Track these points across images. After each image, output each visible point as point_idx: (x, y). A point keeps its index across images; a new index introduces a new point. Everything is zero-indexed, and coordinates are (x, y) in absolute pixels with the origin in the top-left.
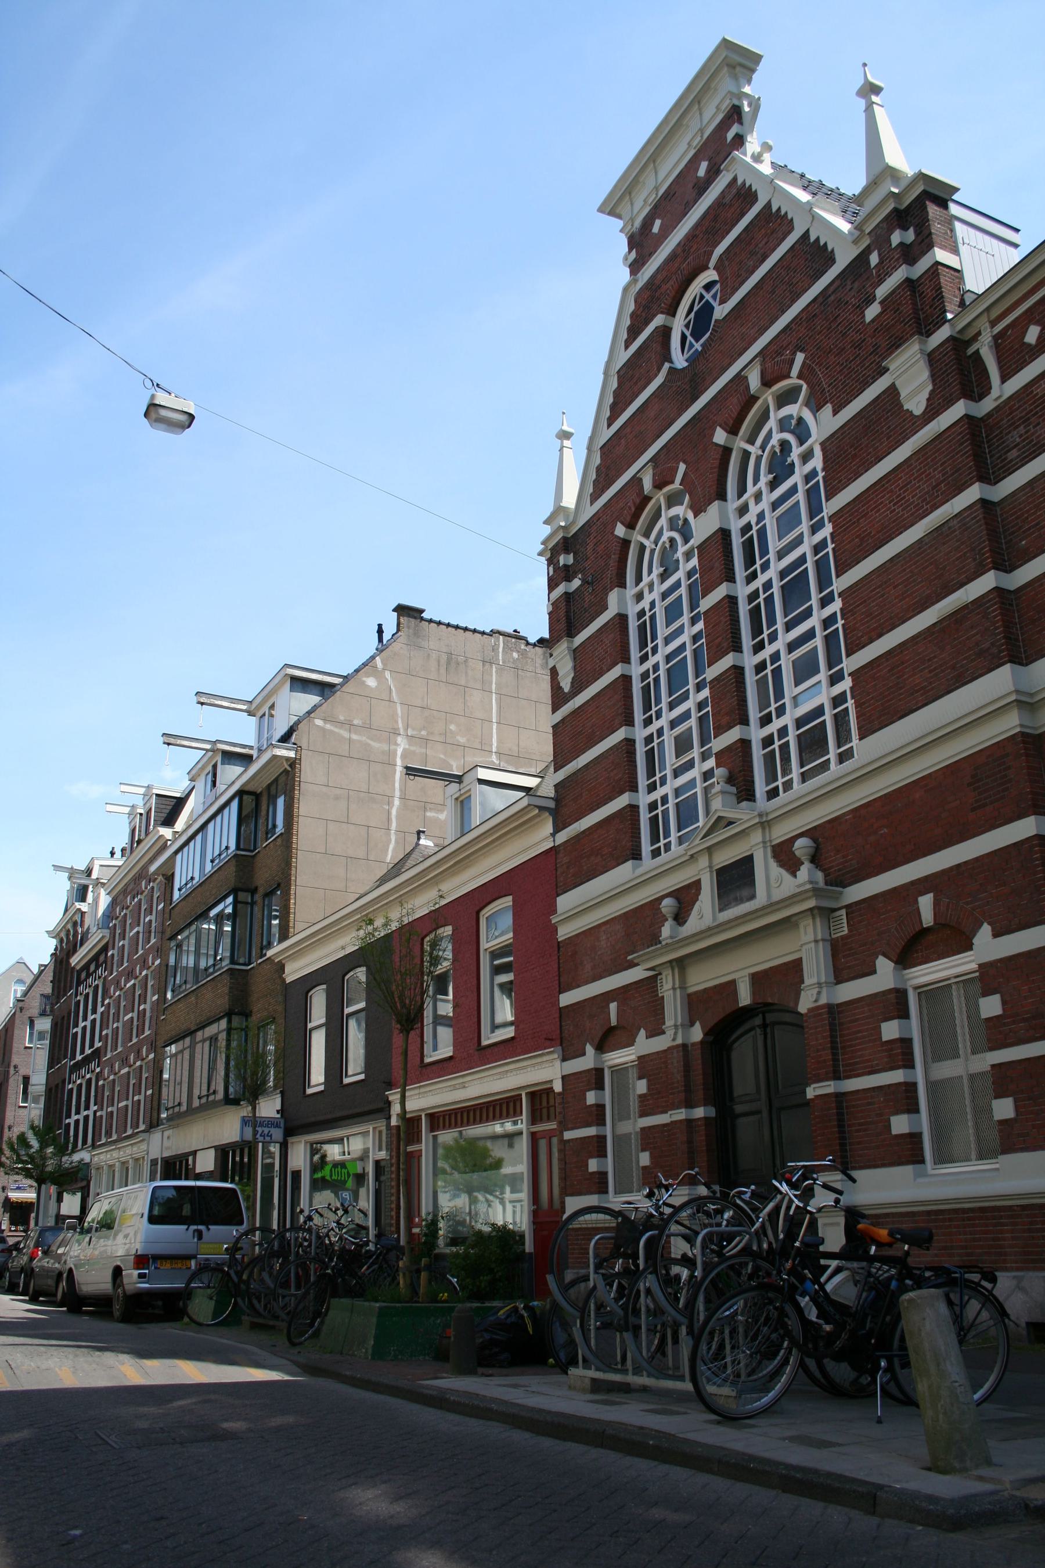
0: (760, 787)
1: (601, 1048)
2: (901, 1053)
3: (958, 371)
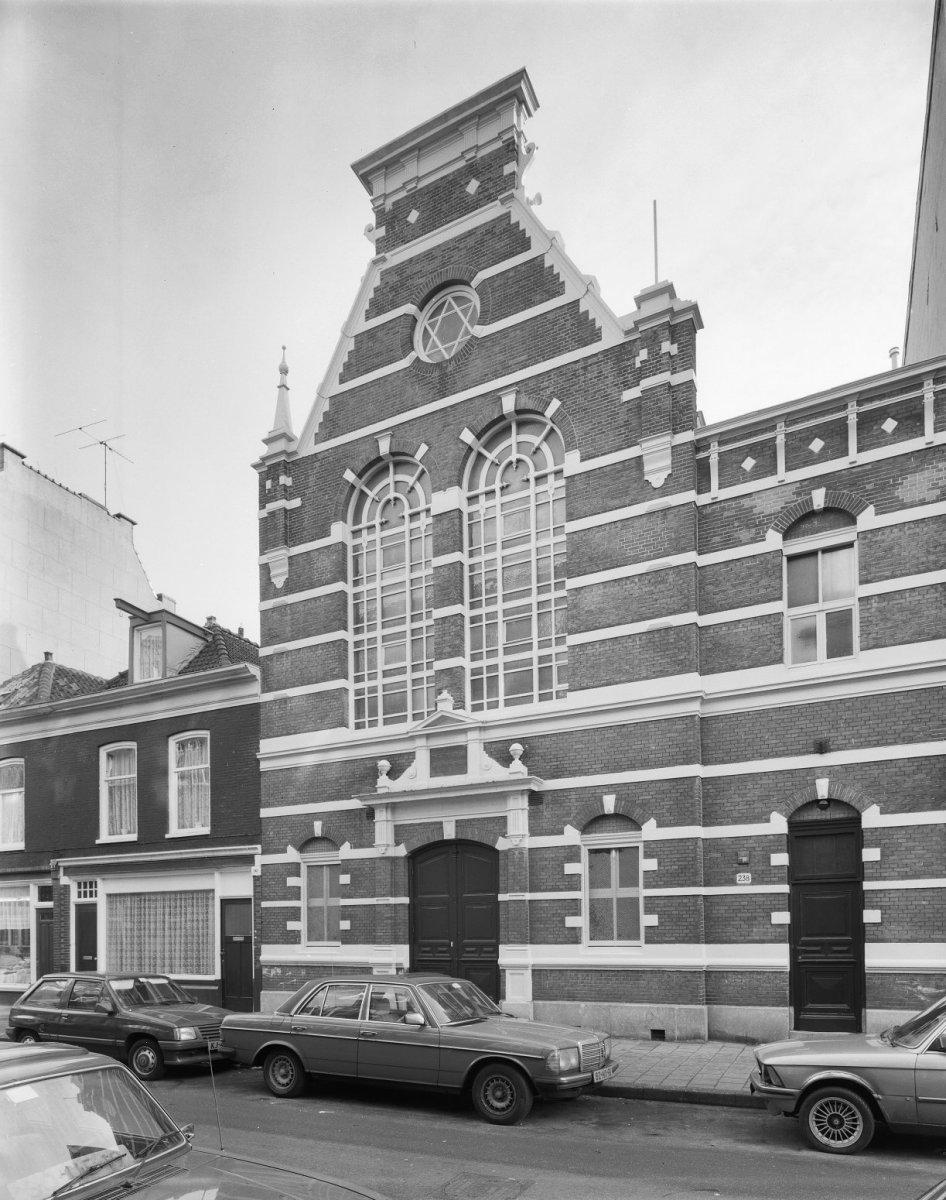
0: (469, 702)
2: (295, 893)
3: (694, 469)
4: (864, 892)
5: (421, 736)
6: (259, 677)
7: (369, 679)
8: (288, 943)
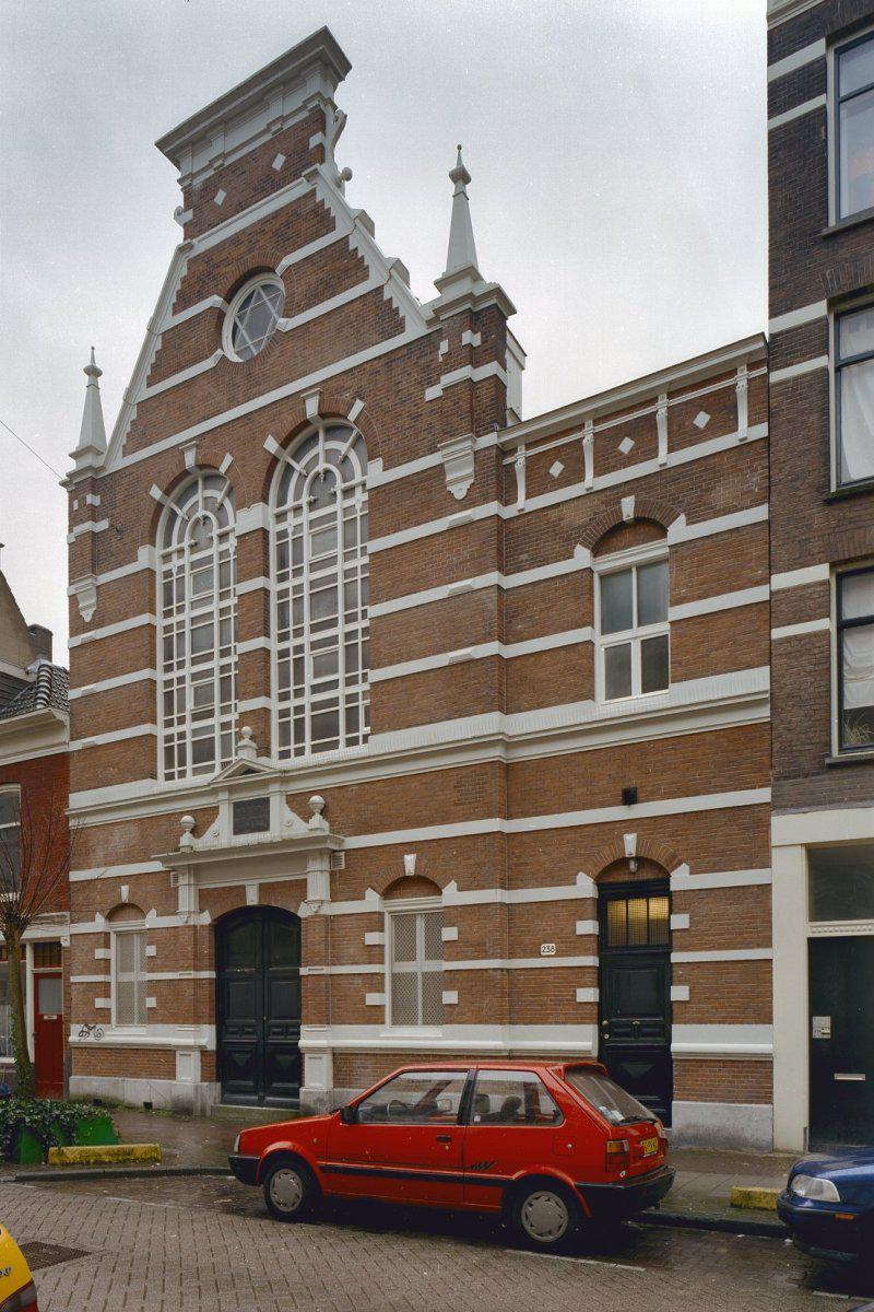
0: (275, 748)
1: (110, 917)
2: (375, 953)
3: (495, 478)
4: (672, 964)
5: (223, 789)
6: (67, 723)
7: (296, 697)
8: (480, 1023)
